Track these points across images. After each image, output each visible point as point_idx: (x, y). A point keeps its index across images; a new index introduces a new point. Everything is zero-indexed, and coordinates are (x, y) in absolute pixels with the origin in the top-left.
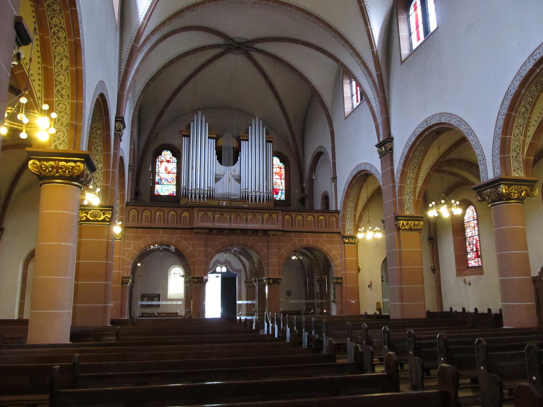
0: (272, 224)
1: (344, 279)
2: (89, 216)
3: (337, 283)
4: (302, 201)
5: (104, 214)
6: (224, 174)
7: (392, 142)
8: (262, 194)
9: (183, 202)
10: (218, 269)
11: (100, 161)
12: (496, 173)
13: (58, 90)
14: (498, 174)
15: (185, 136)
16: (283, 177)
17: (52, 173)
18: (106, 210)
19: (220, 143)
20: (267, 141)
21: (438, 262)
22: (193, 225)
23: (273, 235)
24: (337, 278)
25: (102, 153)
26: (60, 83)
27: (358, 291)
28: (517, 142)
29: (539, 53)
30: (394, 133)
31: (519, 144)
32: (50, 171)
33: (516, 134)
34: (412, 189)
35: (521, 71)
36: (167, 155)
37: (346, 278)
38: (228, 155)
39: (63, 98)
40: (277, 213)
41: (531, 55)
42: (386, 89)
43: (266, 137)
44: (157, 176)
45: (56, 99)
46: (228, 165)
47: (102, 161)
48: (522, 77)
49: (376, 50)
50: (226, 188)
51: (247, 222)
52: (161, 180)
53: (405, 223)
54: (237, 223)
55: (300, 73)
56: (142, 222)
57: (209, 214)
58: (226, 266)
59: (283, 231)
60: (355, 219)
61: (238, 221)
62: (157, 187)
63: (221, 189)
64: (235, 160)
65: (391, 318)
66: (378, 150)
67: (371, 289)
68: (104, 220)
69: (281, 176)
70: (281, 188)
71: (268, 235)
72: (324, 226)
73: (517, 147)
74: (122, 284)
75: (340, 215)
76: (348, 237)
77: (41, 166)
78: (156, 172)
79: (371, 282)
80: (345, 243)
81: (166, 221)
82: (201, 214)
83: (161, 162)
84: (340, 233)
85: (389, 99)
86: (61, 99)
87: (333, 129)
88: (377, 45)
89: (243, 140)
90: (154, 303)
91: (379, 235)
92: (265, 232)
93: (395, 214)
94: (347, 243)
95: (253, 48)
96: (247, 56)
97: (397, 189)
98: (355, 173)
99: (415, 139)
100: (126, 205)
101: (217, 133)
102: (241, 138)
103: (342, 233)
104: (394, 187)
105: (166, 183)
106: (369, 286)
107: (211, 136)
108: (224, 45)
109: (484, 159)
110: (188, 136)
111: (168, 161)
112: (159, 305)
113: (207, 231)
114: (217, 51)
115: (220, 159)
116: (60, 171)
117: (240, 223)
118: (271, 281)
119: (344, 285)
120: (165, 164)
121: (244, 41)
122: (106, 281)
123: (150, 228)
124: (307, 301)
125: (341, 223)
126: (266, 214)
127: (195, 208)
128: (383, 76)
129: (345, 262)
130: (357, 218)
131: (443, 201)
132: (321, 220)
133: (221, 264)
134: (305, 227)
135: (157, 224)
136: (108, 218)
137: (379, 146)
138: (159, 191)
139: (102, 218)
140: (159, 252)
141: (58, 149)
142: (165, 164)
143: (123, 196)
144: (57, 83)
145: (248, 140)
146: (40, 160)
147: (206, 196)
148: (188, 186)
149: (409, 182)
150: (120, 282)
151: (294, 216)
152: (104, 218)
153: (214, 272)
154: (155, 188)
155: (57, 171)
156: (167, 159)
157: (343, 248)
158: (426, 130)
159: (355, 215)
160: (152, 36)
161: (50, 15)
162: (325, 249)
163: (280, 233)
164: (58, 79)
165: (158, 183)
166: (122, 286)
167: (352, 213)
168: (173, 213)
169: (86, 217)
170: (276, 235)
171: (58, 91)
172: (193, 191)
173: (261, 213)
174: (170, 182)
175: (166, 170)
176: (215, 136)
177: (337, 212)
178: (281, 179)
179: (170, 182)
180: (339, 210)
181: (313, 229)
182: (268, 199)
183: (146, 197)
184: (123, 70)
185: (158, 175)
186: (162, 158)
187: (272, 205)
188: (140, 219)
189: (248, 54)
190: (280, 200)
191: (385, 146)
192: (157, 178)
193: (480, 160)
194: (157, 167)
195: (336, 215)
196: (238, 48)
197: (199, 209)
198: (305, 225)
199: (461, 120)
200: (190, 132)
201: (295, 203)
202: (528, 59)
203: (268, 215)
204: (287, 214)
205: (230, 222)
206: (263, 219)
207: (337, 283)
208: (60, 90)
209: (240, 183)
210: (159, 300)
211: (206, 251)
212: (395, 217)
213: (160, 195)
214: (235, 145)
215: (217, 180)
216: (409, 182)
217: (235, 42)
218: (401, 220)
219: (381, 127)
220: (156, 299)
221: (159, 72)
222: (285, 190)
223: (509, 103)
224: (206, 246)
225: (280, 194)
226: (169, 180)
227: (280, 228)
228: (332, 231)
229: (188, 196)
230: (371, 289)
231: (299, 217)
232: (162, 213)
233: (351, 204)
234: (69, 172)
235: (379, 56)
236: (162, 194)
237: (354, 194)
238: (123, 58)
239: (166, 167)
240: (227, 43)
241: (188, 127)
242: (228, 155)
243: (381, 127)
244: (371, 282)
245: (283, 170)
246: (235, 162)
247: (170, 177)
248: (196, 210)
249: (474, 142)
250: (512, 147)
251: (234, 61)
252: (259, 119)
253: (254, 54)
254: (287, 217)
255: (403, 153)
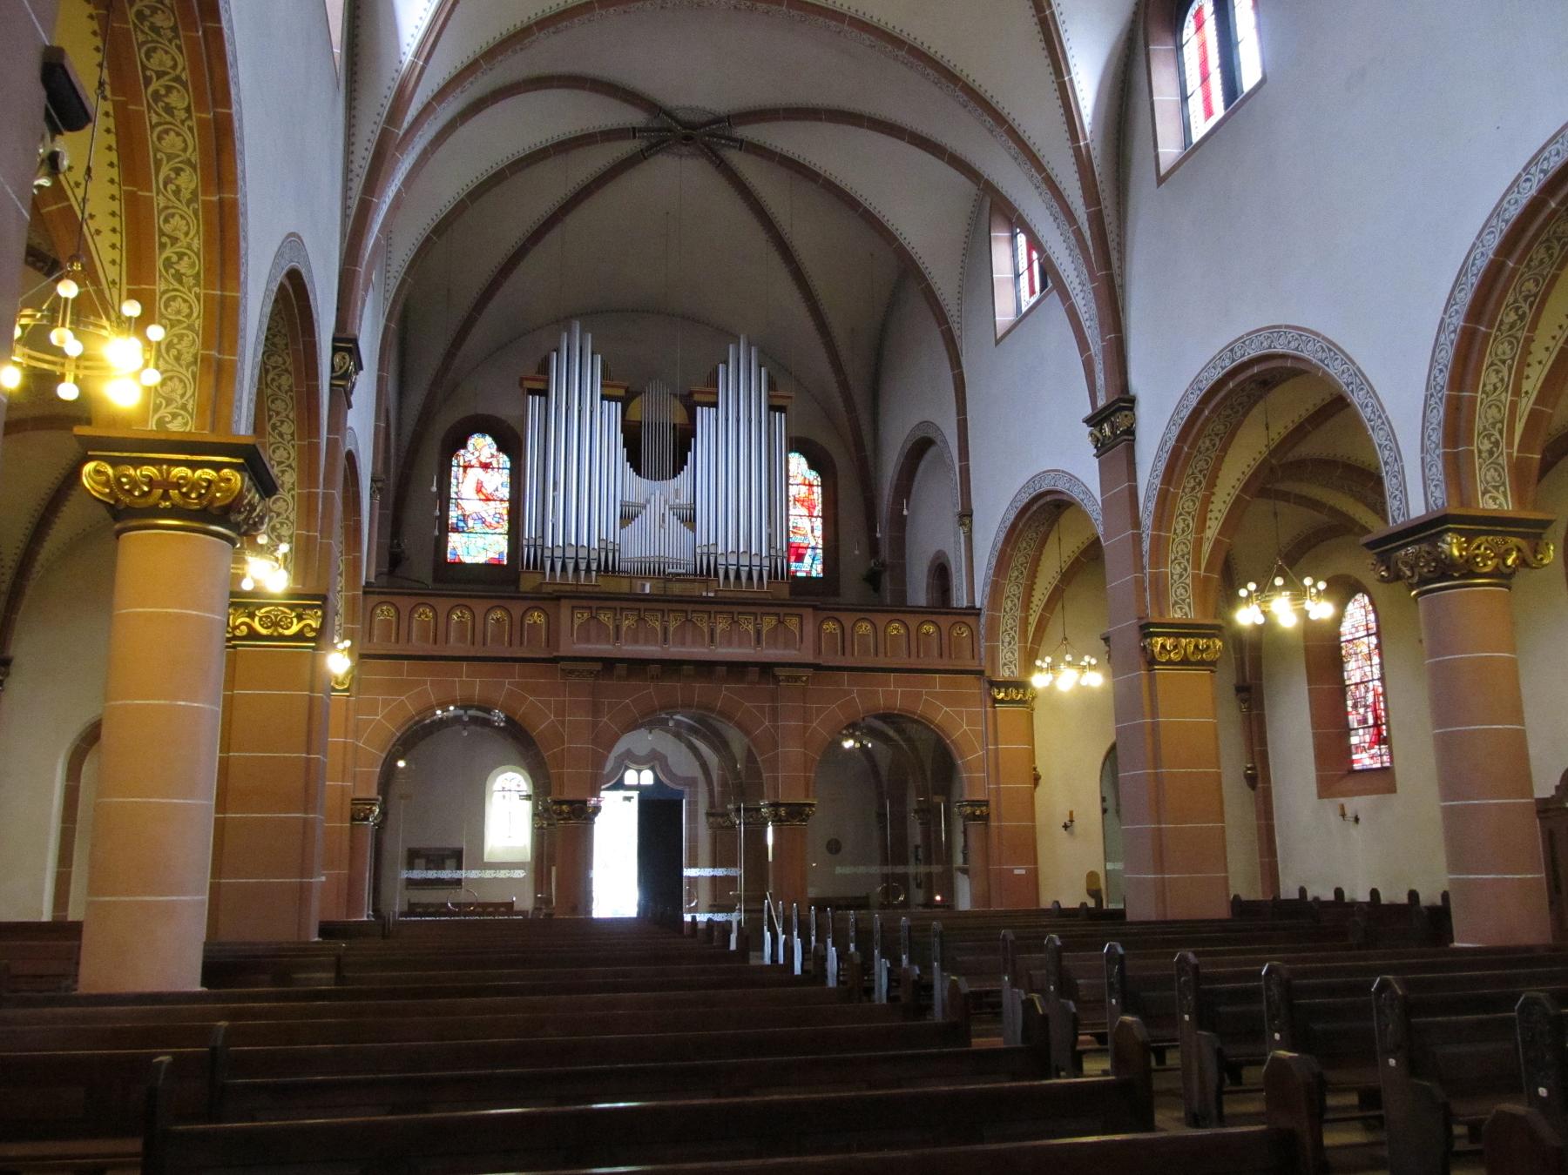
0: (786, 646)
1: (993, 804)
2: (256, 625)
3: (974, 817)
4: (873, 579)
5: (300, 618)
6: (648, 501)
7: (1131, 409)
8: (756, 561)
9: (528, 582)
10: (630, 777)
11: (290, 466)
12: (1431, 501)
13: (168, 259)
14: (1439, 502)
15: (533, 392)
16: (818, 511)
17: (151, 500)
18: (305, 607)
19: (635, 413)
20: (772, 408)
21: (1264, 756)
22: (557, 648)
23: (788, 679)
24: (973, 803)
25: (296, 442)
26: (174, 240)
27: (1034, 840)
28: (1494, 410)
29: (1558, 154)
30: (1137, 384)
31: (1498, 417)
32: (144, 494)
33: (1489, 388)
34: (1191, 547)
35: (1505, 204)
36: (481, 446)
37: (998, 803)
38: (659, 447)
39: (181, 282)
40: (801, 616)
41: (1534, 160)
42: (1114, 256)
43: (769, 397)
44: (452, 507)
45: (163, 287)
46: (659, 476)
47: (294, 464)
48: (1507, 221)
49: (1087, 146)
50: (654, 542)
51: (712, 640)
52: (465, 521)
53: (1169, 643)
54: (683, 644)
55: (866, 211)
56: (409, 640)
57: (604, 617)
58: (652, 769)
59: (817, 667)
60: (1024, 632)
61: (689, 638)
62: (454, 539)
63: (637, 546)
64: (679, 463)
65: (1129, 918)
66: (1091, 434)
67: (1072, 834)
68: (299, 636)
69: (811, 508)
70: (813, 544)
71: (775, 677)
72: (936, 653)
73: (1494, 425)
74: (353, 819)
75: (983, 620)
76: (1006, 685)
77: (118, 480)
78: (449, 498)
79: (1071, 813)
80: (995, 701)
81: (479, 637)
82: (581, 617)
83: (465, 468)
84: (981, 673)
85: (1122, 286)
86: (177, 286)
87: (961, 374)
88: (1088, 128)
89: (703, 405)
90: (446, 874)
91: (1096, 680)
92: (766, 669)
93: (1140, 618)
94: (1002, 701)
95: (730, 139)
96: (712, 162)
97: (1146, 545)
98: (1026, 498)
99: (1200, 403)
100: (365, 593)
101: (626, 384)
102: (697, 397)
103: (988, 673)
104: (1137, 539)
105: (479, 527)
106: (1066, 827)
107: (609, 391)
108: (647, 129)
109: (1398, 458)
110: (544, 393)
111: (486, 466)
112: (458, 882)
113: (598, 666)
114: (626, 148)
115: (635, 459)
116: (173, 493)
117: (694, 643)
118: (782, 812)
119: (993, 824)
120: (476, 474)
121: (705, 119)
122: (306, 811)
123: (433, 658)
124: (888, 869)
125: (983, 643)
126: (767, 619)
127: (563, 602)
128: (1107, 220)
129: (997, 758)
130: (1031, 629)
131: (1279, 581)
132: (927, 634)
133: (639, 762)
134: (881, 655)
135: (455, 647)
136: (313, 630)
137: (1094, 421)
138: (459, 552)
139: (295, 628)
140: (458, 727)
141: (167, 431)
142: (476, 474)
143: (355, 565)
144: (165, 239)
145: (715, 405)
146: (114, 463)
147: (594, 566)
148: (543, 537)
149: (1182, 525)
150: (348, 815)
151: (848, 625)
152: (301, 630)
153: (619, 785)
154: (446, 542)
155: (166, 493)
156: (484, 460)
157: (990, 715)
158: (1231, 374)
159: (1025, 622)
160: (439, 103)
161: (144, 43)
162: (938, 719)
163: (810, 672)
164: (167, 228)
165: (456, 530)
166: (352, 827)
167: (1018, 614)
168: (498, 614)
169: (250, 627)
170: (797, 679)
171: (168, 264)
172: (559, 553)
173: (755, 614)
174: (490, 526)
175: (479, 490)
176: (621, 392)
177: (973, 611)
178: (811, 516)
179: (490, 526)
180: (978, 605)
181: (903, 661)
182: (774, 574)
183: (422, 569)
184: (354, 204)
185: (457, 505)
186: (469, 457)
187: (784, 592)
188: (403, 633)
189: (718, 157)
190: (809, 578)
191: (1113, 422)
192: (454, 514)
193: (1386, 463)
194: (454, 481)
195: (970, 620)
196: (688, 138)
197: (575, 602)
198: (881, 649)
199: (1332, 347)
200: (548, 382)
201: (852, 587)
202: (1525, 169)
203: (773, 621)
204: (828, 618)
205: (665, 640)
206: (758, 633)
207: (974, 817)
208: (175, 258)
209: (694, 529)
210: (459, 867)
211: (595, 725)
212: (1142, 627)
213: (461, 564)
214: (680, 417)
215: (627, 519)
216: (1182, 525)
217: (678, 121)
218: (1158, 635)
219: (1099, 367)
220: (451, 862)
221: (460, 209)
222: (824, 549)
223: (1470, 296)
224: (596, 710)
225: (808, 560)
226: (489, 519)
227: (810, 659)
228: (959, 665)
229: (543, 567)
230: (1072, 834)
231: (865, 628)
232: (467, 615)
233: (1013, 590)
234: (200, 496)
235: (1096, 162)
236: (468, 560)
237: (1022, 560)
238: (355, 167)
239: (478, 482)
240: (656, 124)
241: (544, 368)
242: (659, 447)
243: (1099, 367)
244: (1071, 813)
245: (818, 490)
246: (678, 468)
247: (492, 512)
248: (565, 606)
249: (1369, 410)
250: (1478, 425)
251: (677, 177)
252: (749, 345)
253: (735, 157)
254: (830, 626)
255: (1164, 442)
